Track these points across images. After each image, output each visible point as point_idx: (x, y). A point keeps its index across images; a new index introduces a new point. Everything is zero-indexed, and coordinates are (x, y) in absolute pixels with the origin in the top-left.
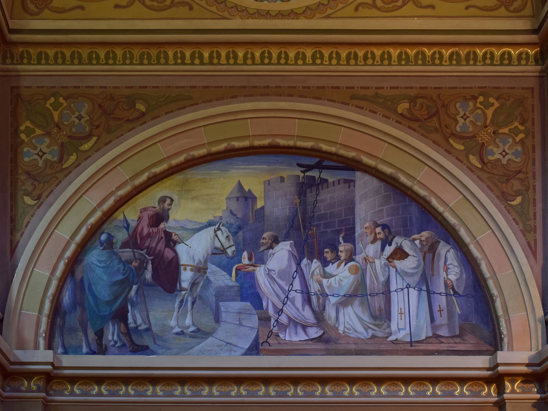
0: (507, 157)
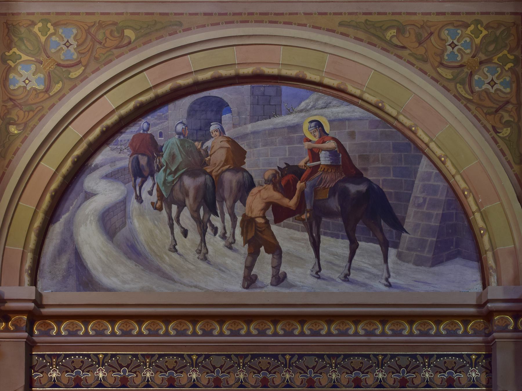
0: (495, 87)
